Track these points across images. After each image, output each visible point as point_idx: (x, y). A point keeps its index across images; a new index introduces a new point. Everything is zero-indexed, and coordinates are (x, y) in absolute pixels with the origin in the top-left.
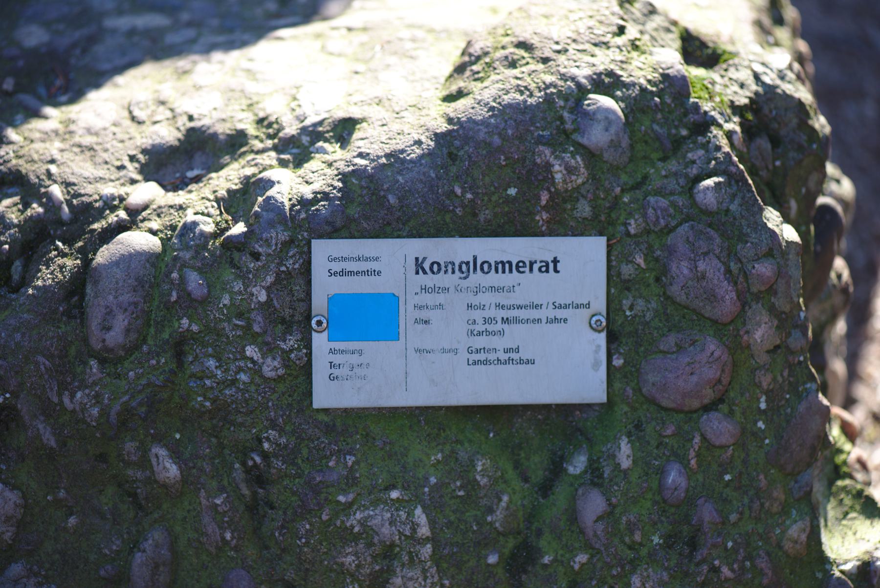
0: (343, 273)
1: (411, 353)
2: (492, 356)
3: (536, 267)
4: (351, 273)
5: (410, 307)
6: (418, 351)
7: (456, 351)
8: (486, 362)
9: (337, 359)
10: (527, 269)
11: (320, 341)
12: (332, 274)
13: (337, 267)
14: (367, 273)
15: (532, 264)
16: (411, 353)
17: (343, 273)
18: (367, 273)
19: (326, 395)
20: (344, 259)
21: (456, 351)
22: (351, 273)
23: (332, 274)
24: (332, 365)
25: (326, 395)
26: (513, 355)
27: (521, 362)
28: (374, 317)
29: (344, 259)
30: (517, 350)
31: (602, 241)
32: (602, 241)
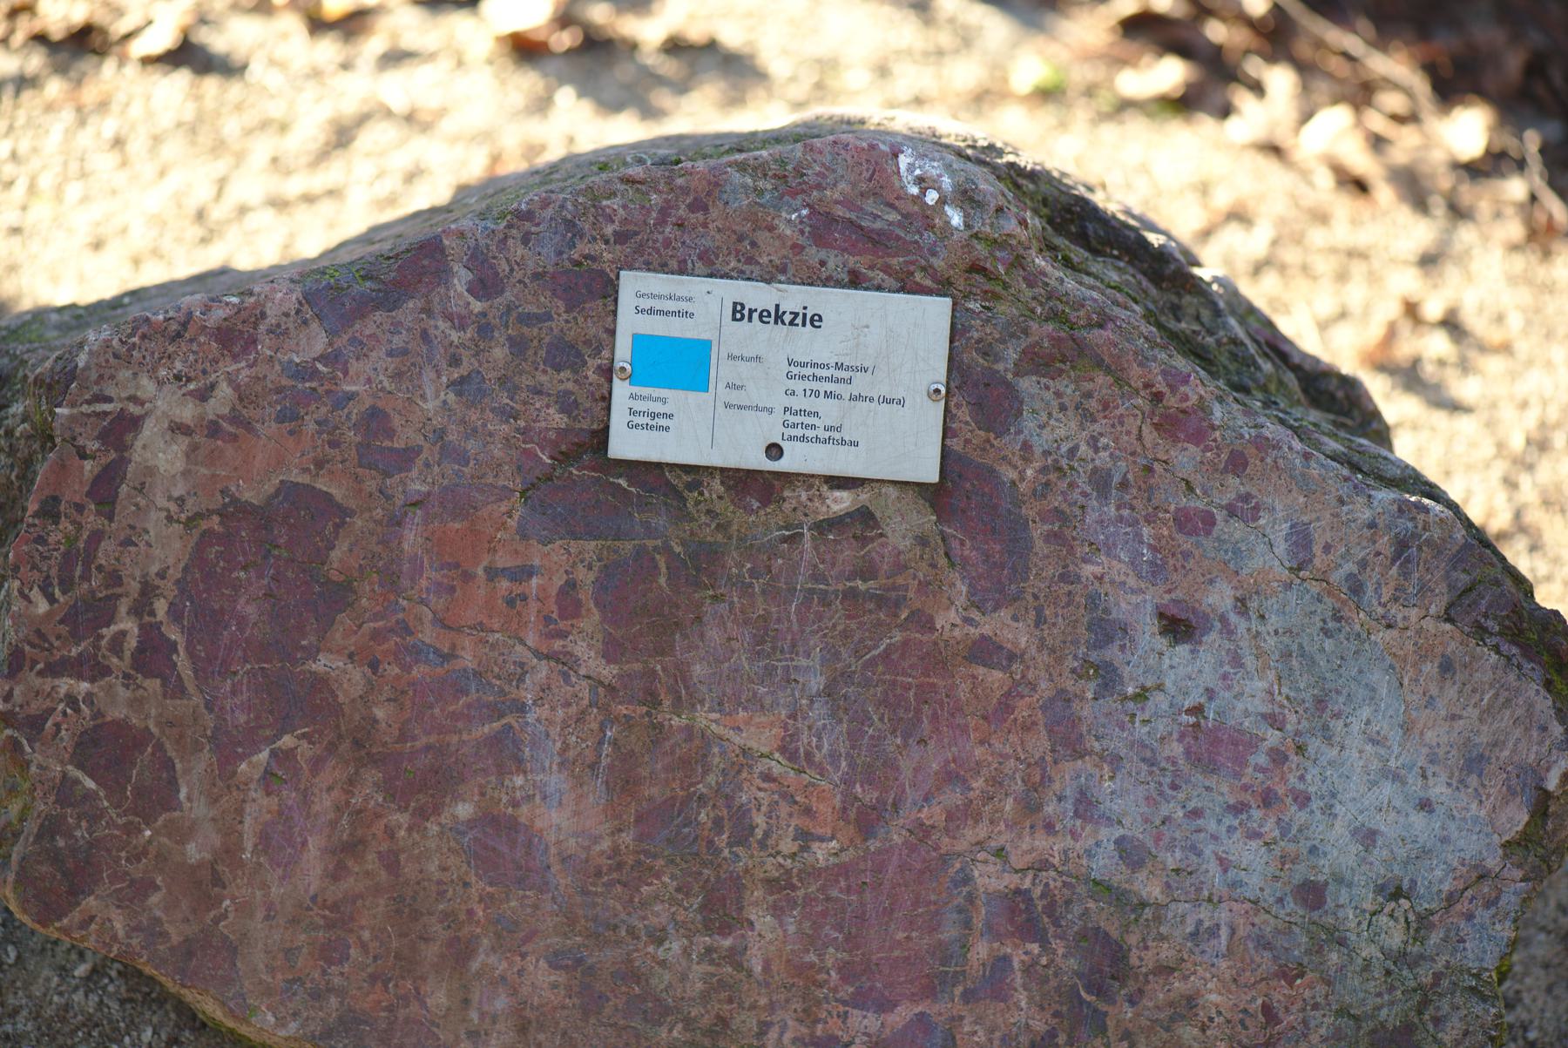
0: (651, 311)
1: (720, 405)
2: (810, 433)
3: (755, 316)
4: (661, 312)
5: (721, 386)
6: (731, 357)
7: (770, 411)
8: (803, 439)
9: (640, 406)
10: (772, 320)
11: (621, 391)
12: (638, 311)
13: (646, 304)
14: (678, 313)
15: (751, 311)
16: (720, 408)
17: (651, 311)
18: (678, 313)
19: (625, 444)
20: (653, 296)
21: (770, 411)
22: (661, 312)
23: (638, 311)
24: (632, 412)
25: (625, 444)
26: (837, 436)
27: (843, 442)
28: (686, 365)
29: (653, 296)
30: (838, 429)
31: (948, 301)
32: (948, 301)
